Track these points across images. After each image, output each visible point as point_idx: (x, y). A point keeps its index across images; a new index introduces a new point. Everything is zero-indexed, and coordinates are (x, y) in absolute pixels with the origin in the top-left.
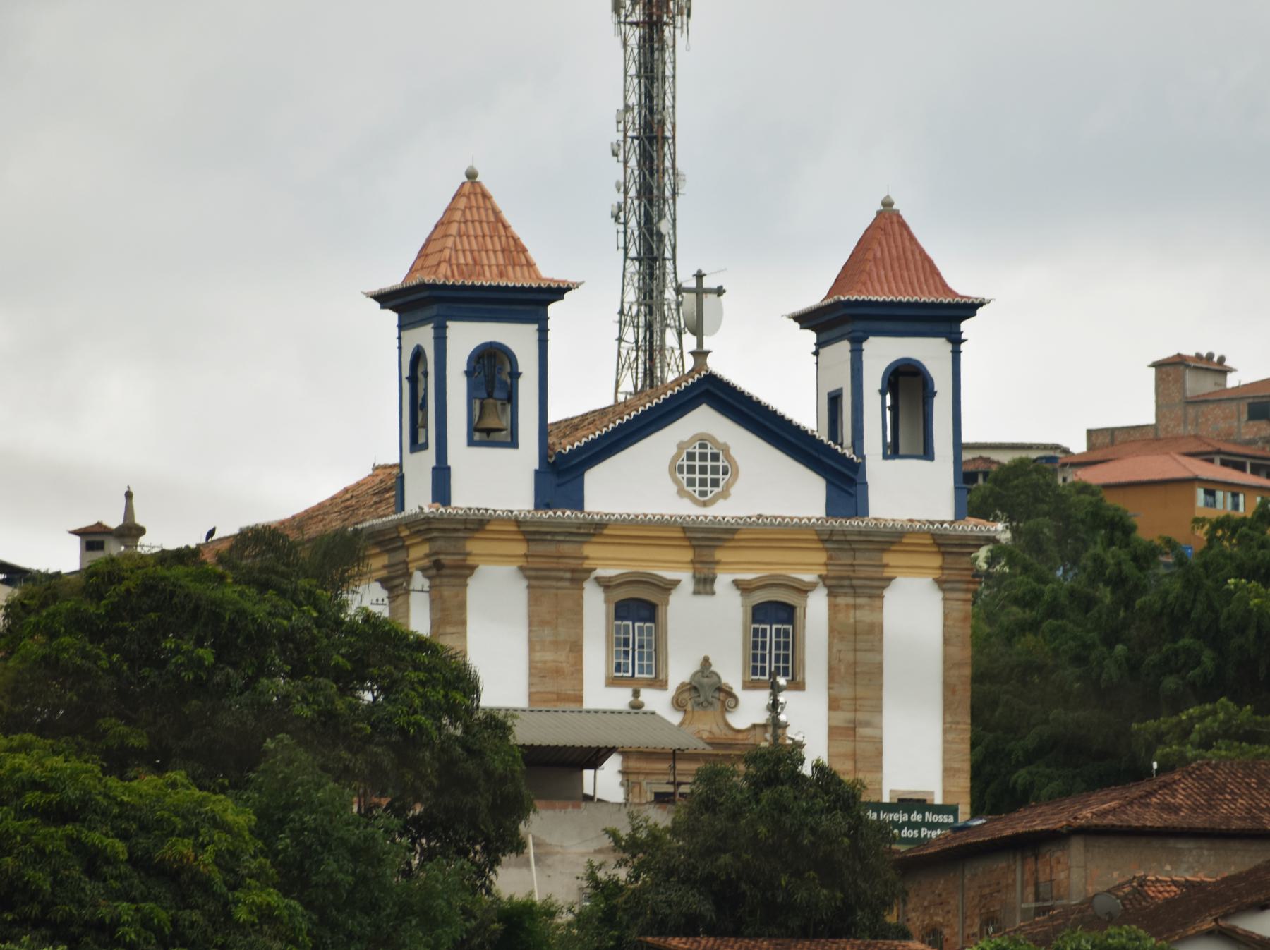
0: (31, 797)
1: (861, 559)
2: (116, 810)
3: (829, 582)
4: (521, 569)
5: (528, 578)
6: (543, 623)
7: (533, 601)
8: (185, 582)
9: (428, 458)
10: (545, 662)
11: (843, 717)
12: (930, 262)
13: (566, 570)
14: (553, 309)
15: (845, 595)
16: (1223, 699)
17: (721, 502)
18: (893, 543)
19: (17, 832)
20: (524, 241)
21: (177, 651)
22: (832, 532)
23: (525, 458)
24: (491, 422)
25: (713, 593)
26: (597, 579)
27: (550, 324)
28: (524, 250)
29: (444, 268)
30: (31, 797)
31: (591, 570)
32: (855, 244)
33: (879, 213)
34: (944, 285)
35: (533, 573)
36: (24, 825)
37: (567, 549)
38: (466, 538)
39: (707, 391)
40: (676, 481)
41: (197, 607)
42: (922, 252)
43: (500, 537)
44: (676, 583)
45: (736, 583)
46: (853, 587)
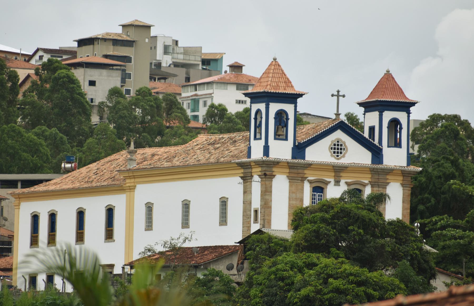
0: (351, 278)
1: (381, 177)
2: (373, 283)
3: (372, 183)
4: (288, 176)
5: (289, 179)
6: (293, 193)
7: (291, 186)
8: (353, 209)
9: (262, 142)
10: (293, 204)
12: (401, 89)
13: (300, 177)
14: (299, 100)
15: (376, 187)
16: (446, 215)
17: (343, 159)
18: (390, 172)
19: (351, 289)
20: (291, 79)
21: (354, 230)
22: (374, 169)
23: (290, 144)
24: (280, 133)
25: (340, 185)
26: (308, 180)
27: (298, 104)
28: (291, 82)
29: (268, 87)
30: (351, 278)
31: (306, 178)
32: (377, 83)
33: (385, 74)
34: (405, 97)
35: (291, 178)
36: (351, 286)
37: (300, 171)
38: (273, 167)
39: (340, 126)
40: (330, 152)
41: (358, 217)
42: (399, 86)
43: (282, 167)
44: (330, 182)
45: (346, 183)
46: (378, 185)
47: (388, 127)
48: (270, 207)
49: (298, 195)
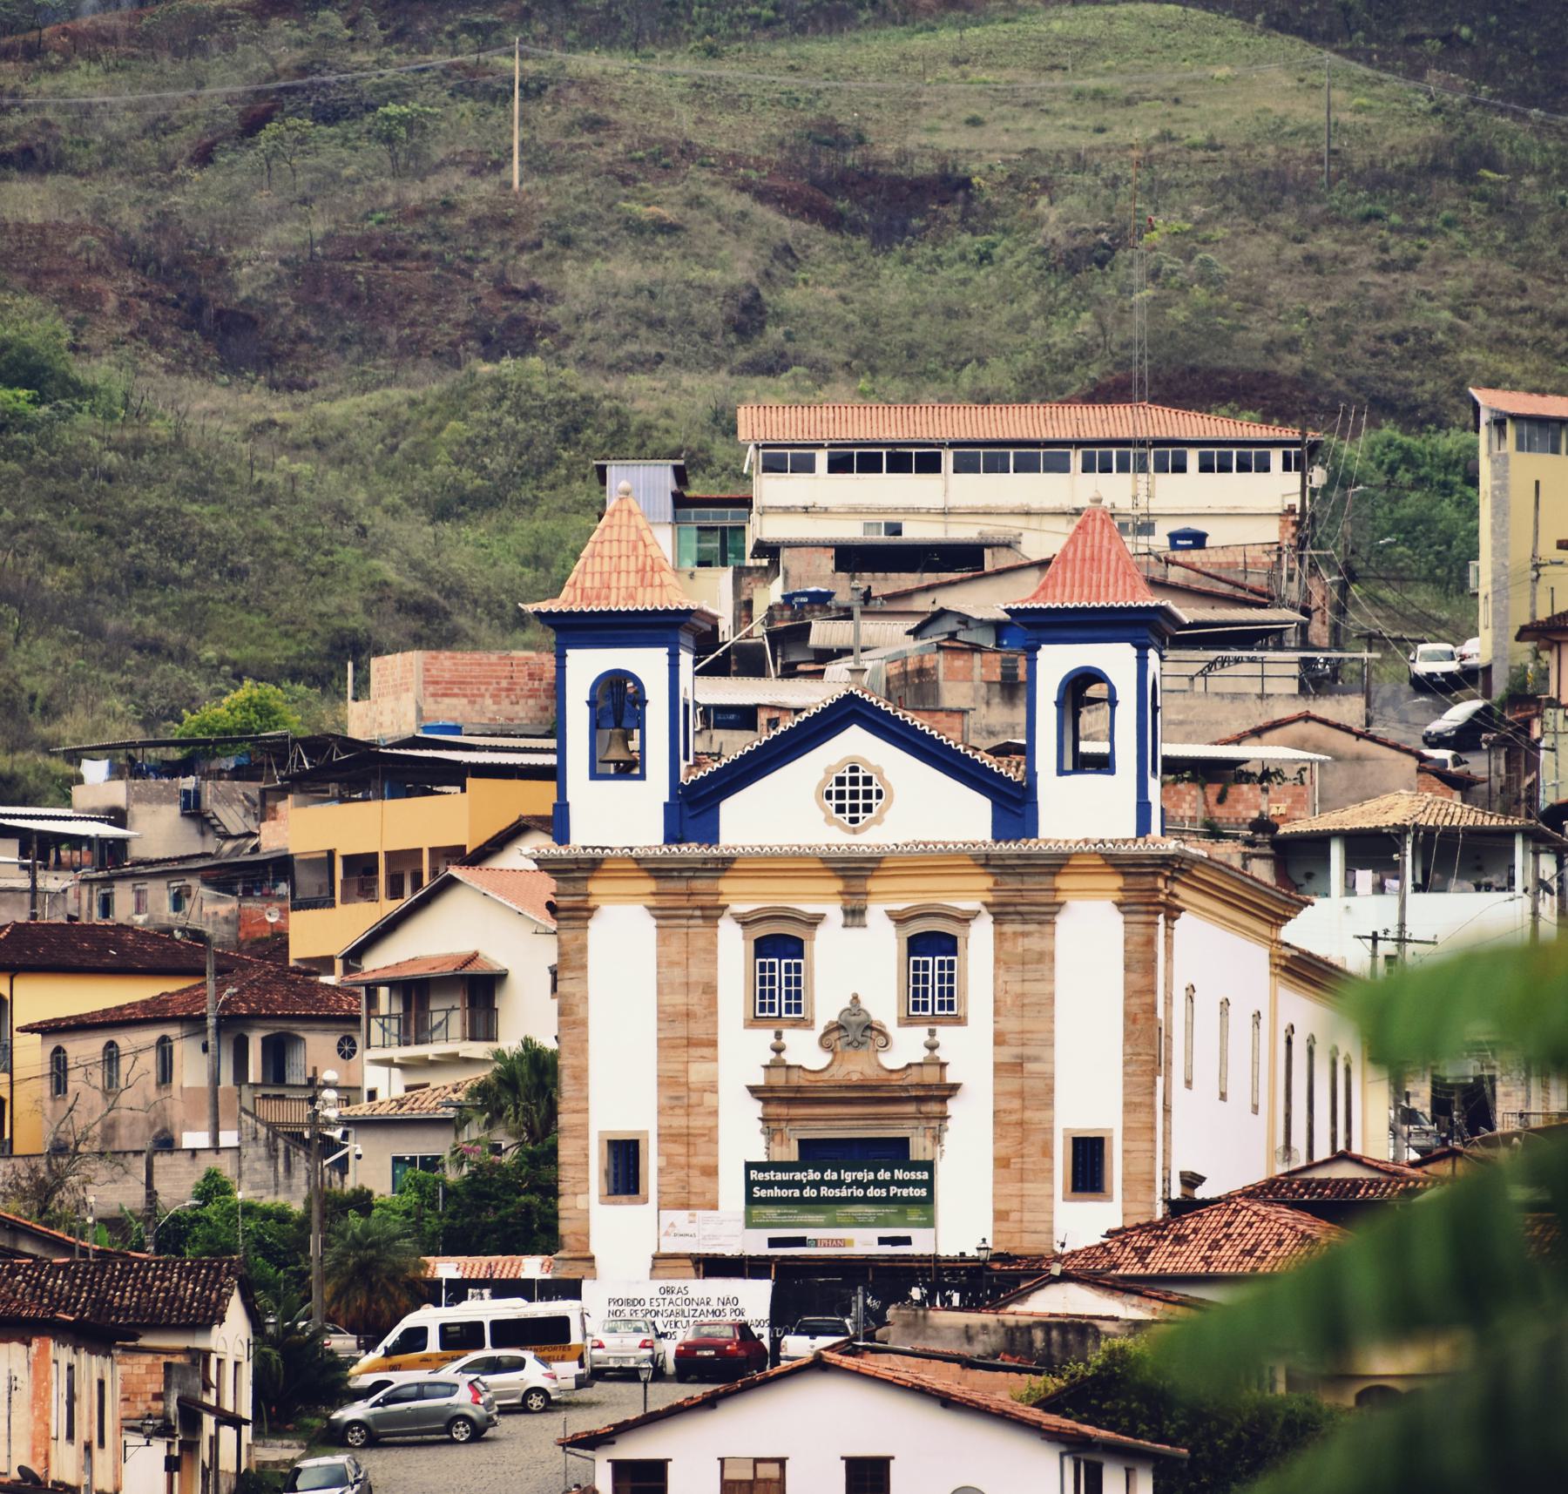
4: (1119, 905)
6: (672, 964)
7: (662, 941)
11: (1008, 1054)
23: (655, 789)
31: (725, 907)
37: (699, 885)
40: (823, 808)
47: (591, 703)
48: (584, 1023)
49: (697, 973)
